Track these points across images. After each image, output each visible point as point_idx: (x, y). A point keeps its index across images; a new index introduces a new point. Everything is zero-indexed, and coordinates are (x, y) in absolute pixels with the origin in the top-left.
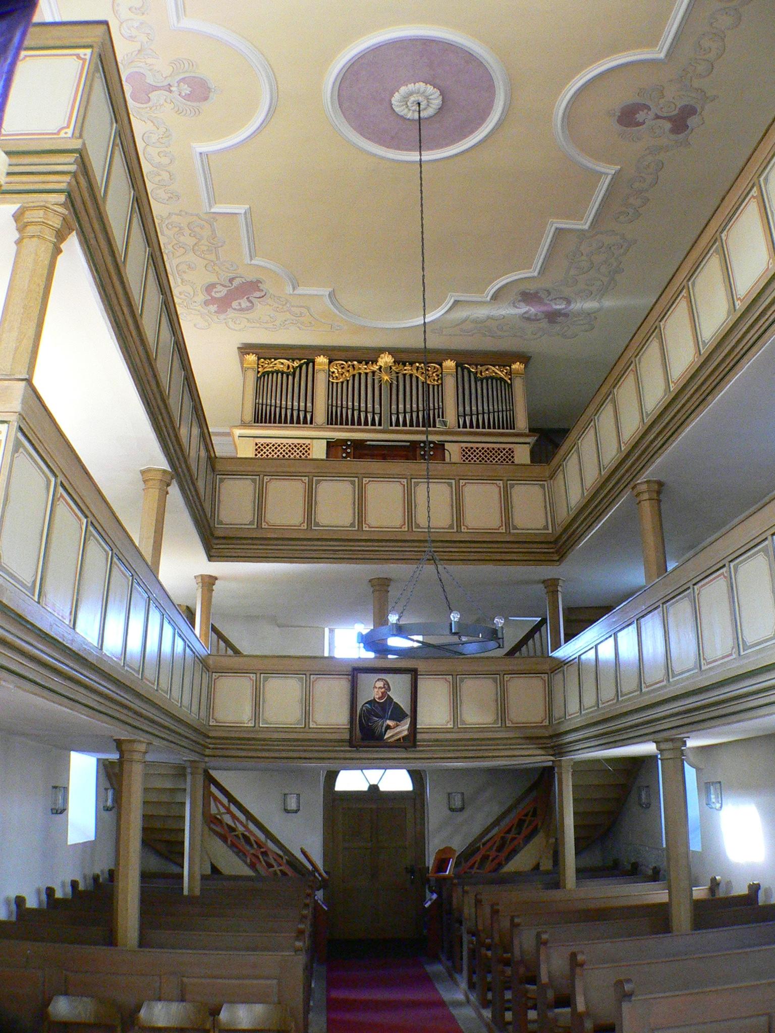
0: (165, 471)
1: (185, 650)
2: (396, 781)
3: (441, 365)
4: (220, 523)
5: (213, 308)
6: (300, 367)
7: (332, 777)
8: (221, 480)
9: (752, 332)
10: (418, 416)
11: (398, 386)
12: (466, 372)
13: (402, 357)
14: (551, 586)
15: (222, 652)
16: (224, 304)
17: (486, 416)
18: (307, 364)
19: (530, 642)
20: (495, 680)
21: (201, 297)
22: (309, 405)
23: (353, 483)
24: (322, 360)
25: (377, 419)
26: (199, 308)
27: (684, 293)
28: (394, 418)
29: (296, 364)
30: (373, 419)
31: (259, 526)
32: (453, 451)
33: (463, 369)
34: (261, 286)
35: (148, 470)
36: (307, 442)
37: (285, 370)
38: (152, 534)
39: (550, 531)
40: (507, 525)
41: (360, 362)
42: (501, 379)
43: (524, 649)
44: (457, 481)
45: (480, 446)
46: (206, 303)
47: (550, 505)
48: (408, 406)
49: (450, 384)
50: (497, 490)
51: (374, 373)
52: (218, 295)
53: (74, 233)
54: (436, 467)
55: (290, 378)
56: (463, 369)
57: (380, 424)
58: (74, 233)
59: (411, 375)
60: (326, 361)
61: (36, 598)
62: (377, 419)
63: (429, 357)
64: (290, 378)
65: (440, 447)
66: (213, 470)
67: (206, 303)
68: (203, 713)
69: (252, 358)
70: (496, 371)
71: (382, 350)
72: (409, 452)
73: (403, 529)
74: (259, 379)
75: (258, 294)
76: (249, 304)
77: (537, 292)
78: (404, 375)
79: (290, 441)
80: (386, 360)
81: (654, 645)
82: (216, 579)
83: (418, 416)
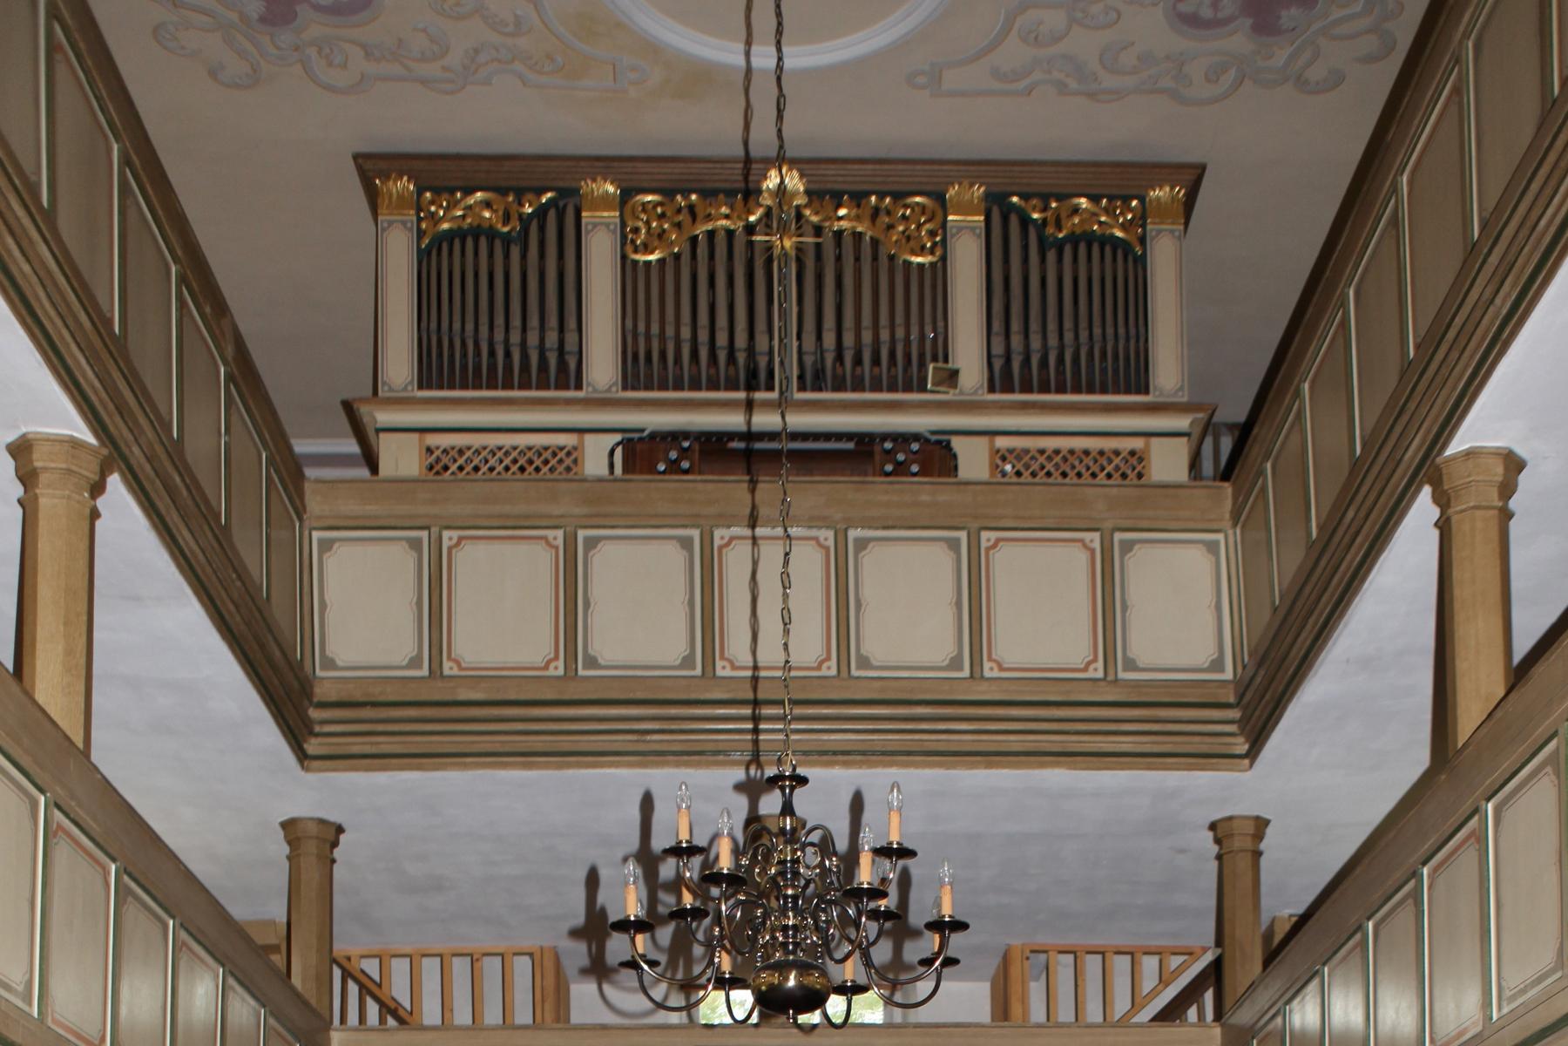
0: (75, 444)
4: (329, 664)
6: (541, 212)
15: (400, 968)
31: (436, 672)
32: (973, 459)
38: (1498, 562)
44: (972, 528)
50: (1082, 557)
54: (924, 492)
55: (515, 252)
56: (1007, 211)
64: (515, 252)
68: (736, 563)
73: (824, 672)
78: (839, 234)
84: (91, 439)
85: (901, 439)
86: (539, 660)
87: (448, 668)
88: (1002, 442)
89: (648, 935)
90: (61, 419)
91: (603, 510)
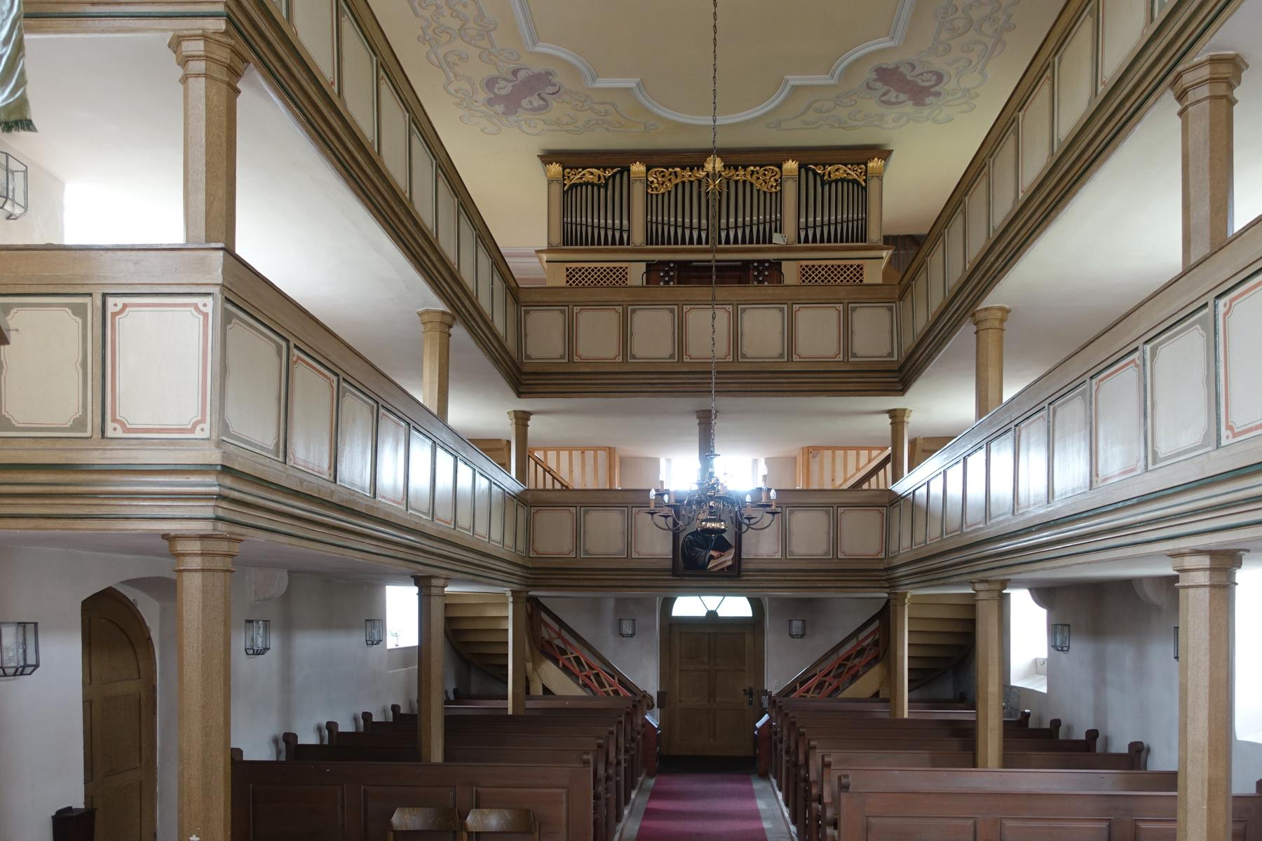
0: (443, 313)
1: (490, 488)
2: (736, 607)
3: (780, 167)
4: (528, 357)
5: (500, 108)
6: (614, 176)
7: (668, 603)
8: (527, 312)
9: (1107, 130)
10: (751, 231)
11: (728, 194)
12: (811, 174)
13: (735, 158)
14: (897, 417)
16: (511, 103)
17: (833, 228)
18: (621, 173)
19: (881, 473)
20: (828, 513)
21: (482, 96)
22: (625, 222)
23: (672, 311)
24: (638, 168)
25: (704, 235)
26: (483, 108)
27: (1048, 73)
28: (723, 234)
29: (608, 174)
30: (700, 236)
32: (791, 272)
33: (807, 170)
34: (554, 80)
35: (427, 312)
36: (624, 265)
37: (596, 181)
39: (895, 358)
40: (846, 353)
41: (683, 168)
42: (854, 181)
43: (874, 479)
44: (789, 305)
45: (823, 263)
46: (490, 102)
47: (897, 330)
48: (740, 220)
49: (790, 190)
50: (835, 314)
51: (700, 181)
52: (503, 92)
53: (252, 65)
54: (768, 290)
55: (602, 191)
57: (707, 243)
58: (252, 65)
59: (744, 182)
60: (643, 168)
61: (281, 459)
62: (704, 235)
63: (772, 157)
64: (602, 191)
65: (776, 265)
66: (517, 301)
67: (490, 102)
68: (521, 546)
69: (555, 169)
70: (841, 172)
71: (707, 153)
72: (738, 273)
74: (565, 193)
75: (551, 89)
76: (542, 103)
77: (897, 67)
78: (737, 182)
79: (605, 265)
80: (714, 164)
81: (1117, 459)
82: (1008, 311)
83: (751, 231)
84: (448, 310)
85: (761, 262)
86: (612, 356)
87: (576, 359)
88: (804, 263)
89: (669, 565)
90: (440, 306)
91: (638, 300)
